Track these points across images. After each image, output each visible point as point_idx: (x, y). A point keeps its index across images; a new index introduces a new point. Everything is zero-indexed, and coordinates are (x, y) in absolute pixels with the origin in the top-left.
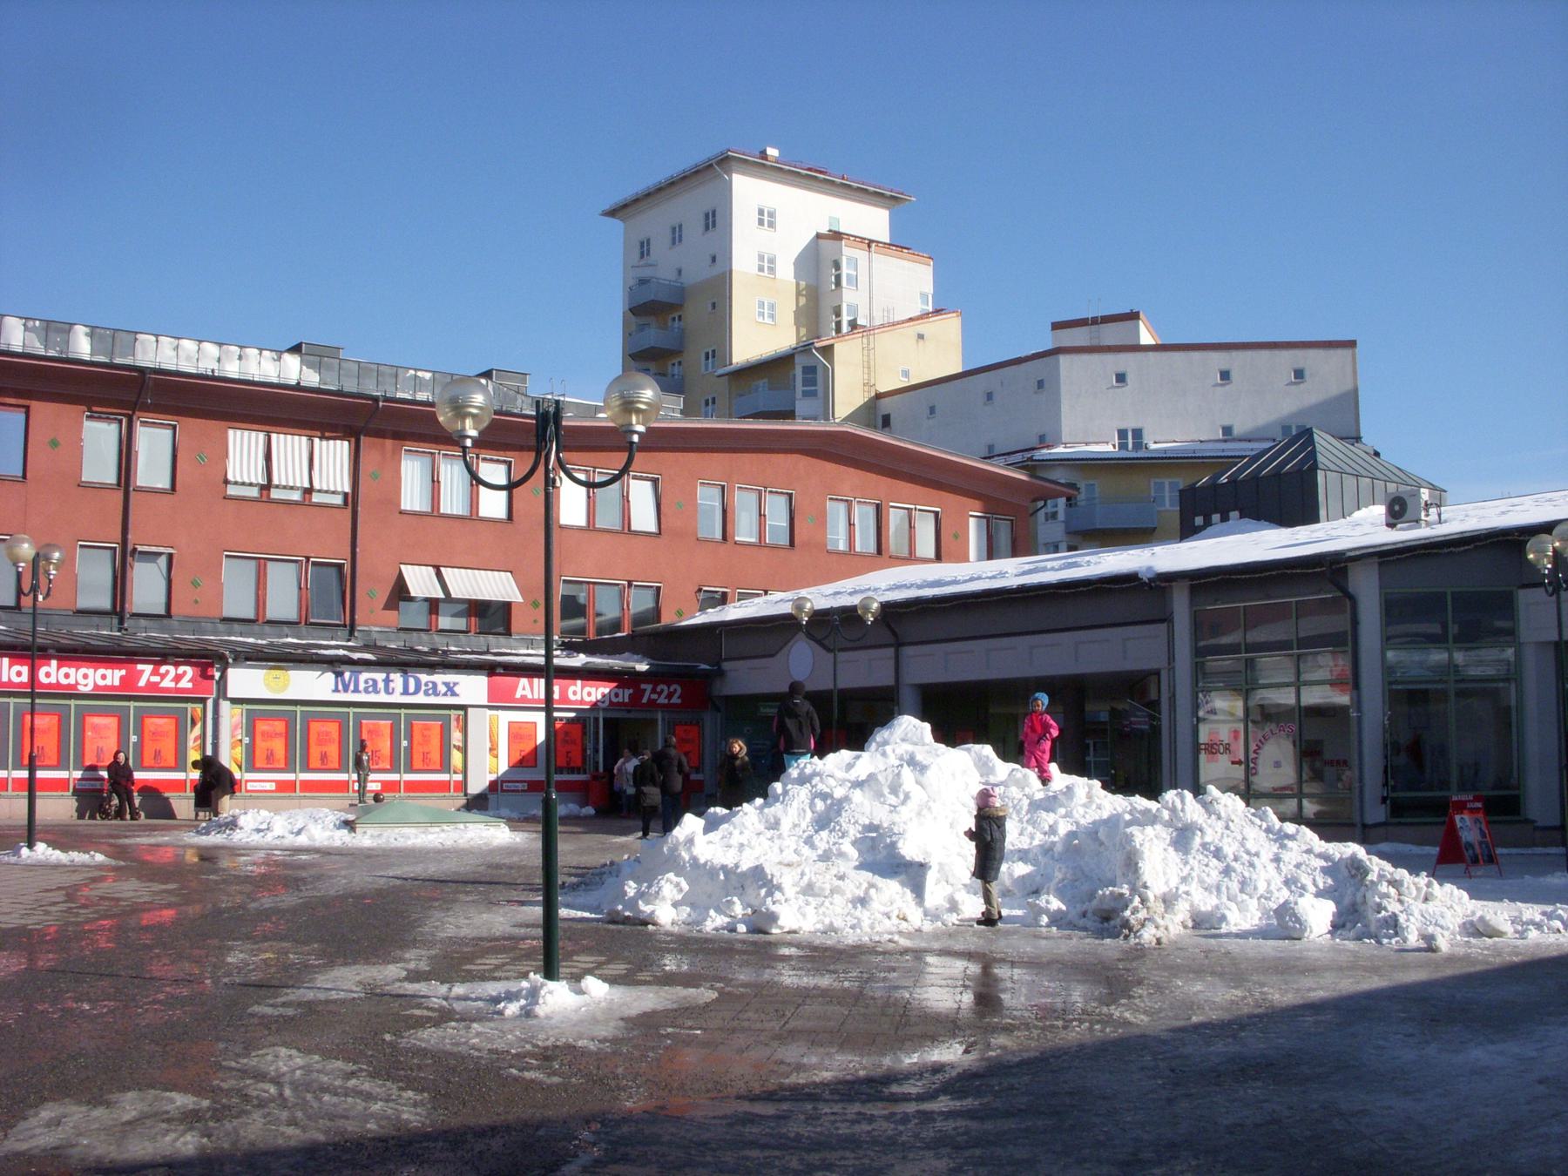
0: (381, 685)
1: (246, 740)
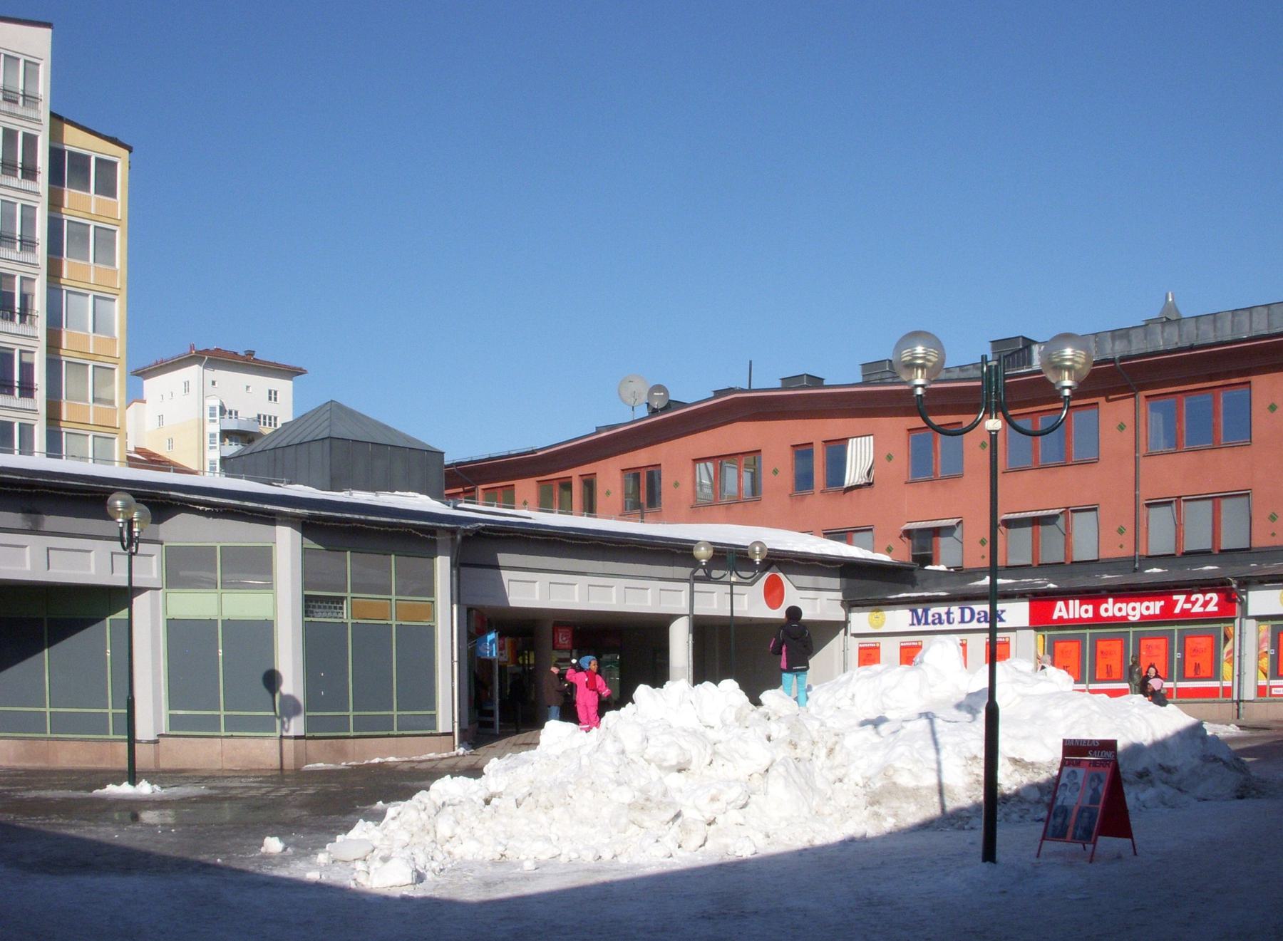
0: (944, 617)
1: (1272, 652)
